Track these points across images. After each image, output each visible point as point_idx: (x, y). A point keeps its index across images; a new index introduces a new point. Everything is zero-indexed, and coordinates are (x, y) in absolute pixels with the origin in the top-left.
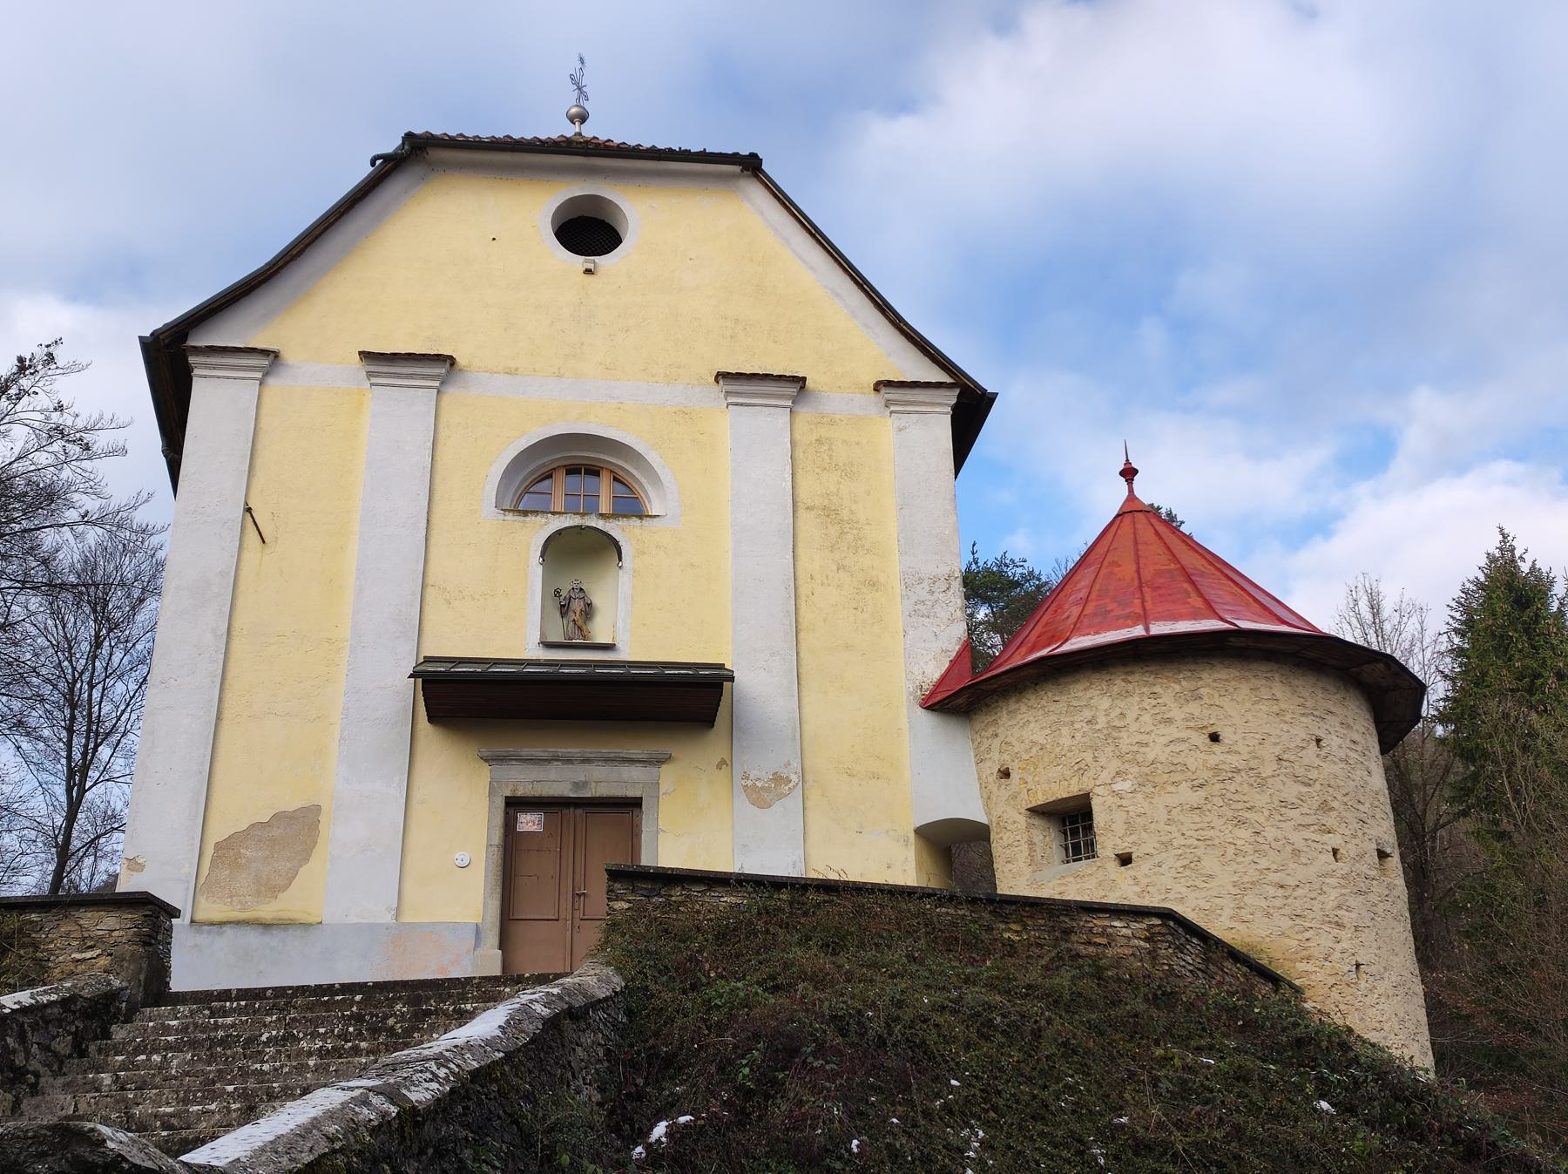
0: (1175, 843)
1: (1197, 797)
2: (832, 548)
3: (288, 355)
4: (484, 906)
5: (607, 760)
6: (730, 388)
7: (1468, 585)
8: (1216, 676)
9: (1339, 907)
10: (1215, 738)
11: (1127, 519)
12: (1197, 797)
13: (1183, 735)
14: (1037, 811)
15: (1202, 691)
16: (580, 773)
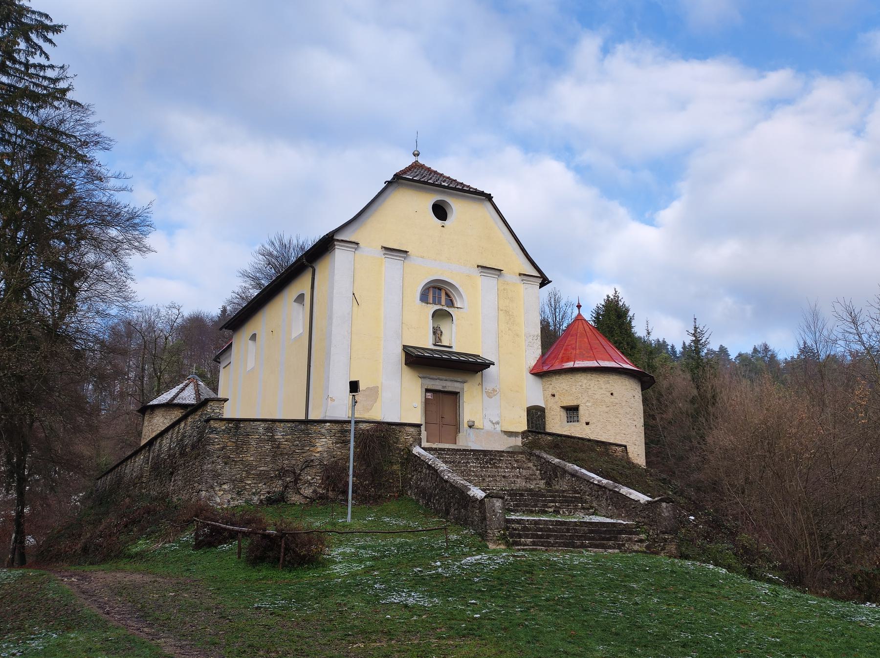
0: (601, 421)
1: (607, 410)
2: (507, 323)
3: (361, 245)
4: (421, 418)
5: (452, 381)
6: (482, 270)
7: (599, 305)
8: (613, 377)
9: (635, 440)
10: (612, 394)
11: (577, 321)
12: (607, 410)
13: (605, 392)
14: (562, 407)
15: (610, 381)
16: (444, 383)
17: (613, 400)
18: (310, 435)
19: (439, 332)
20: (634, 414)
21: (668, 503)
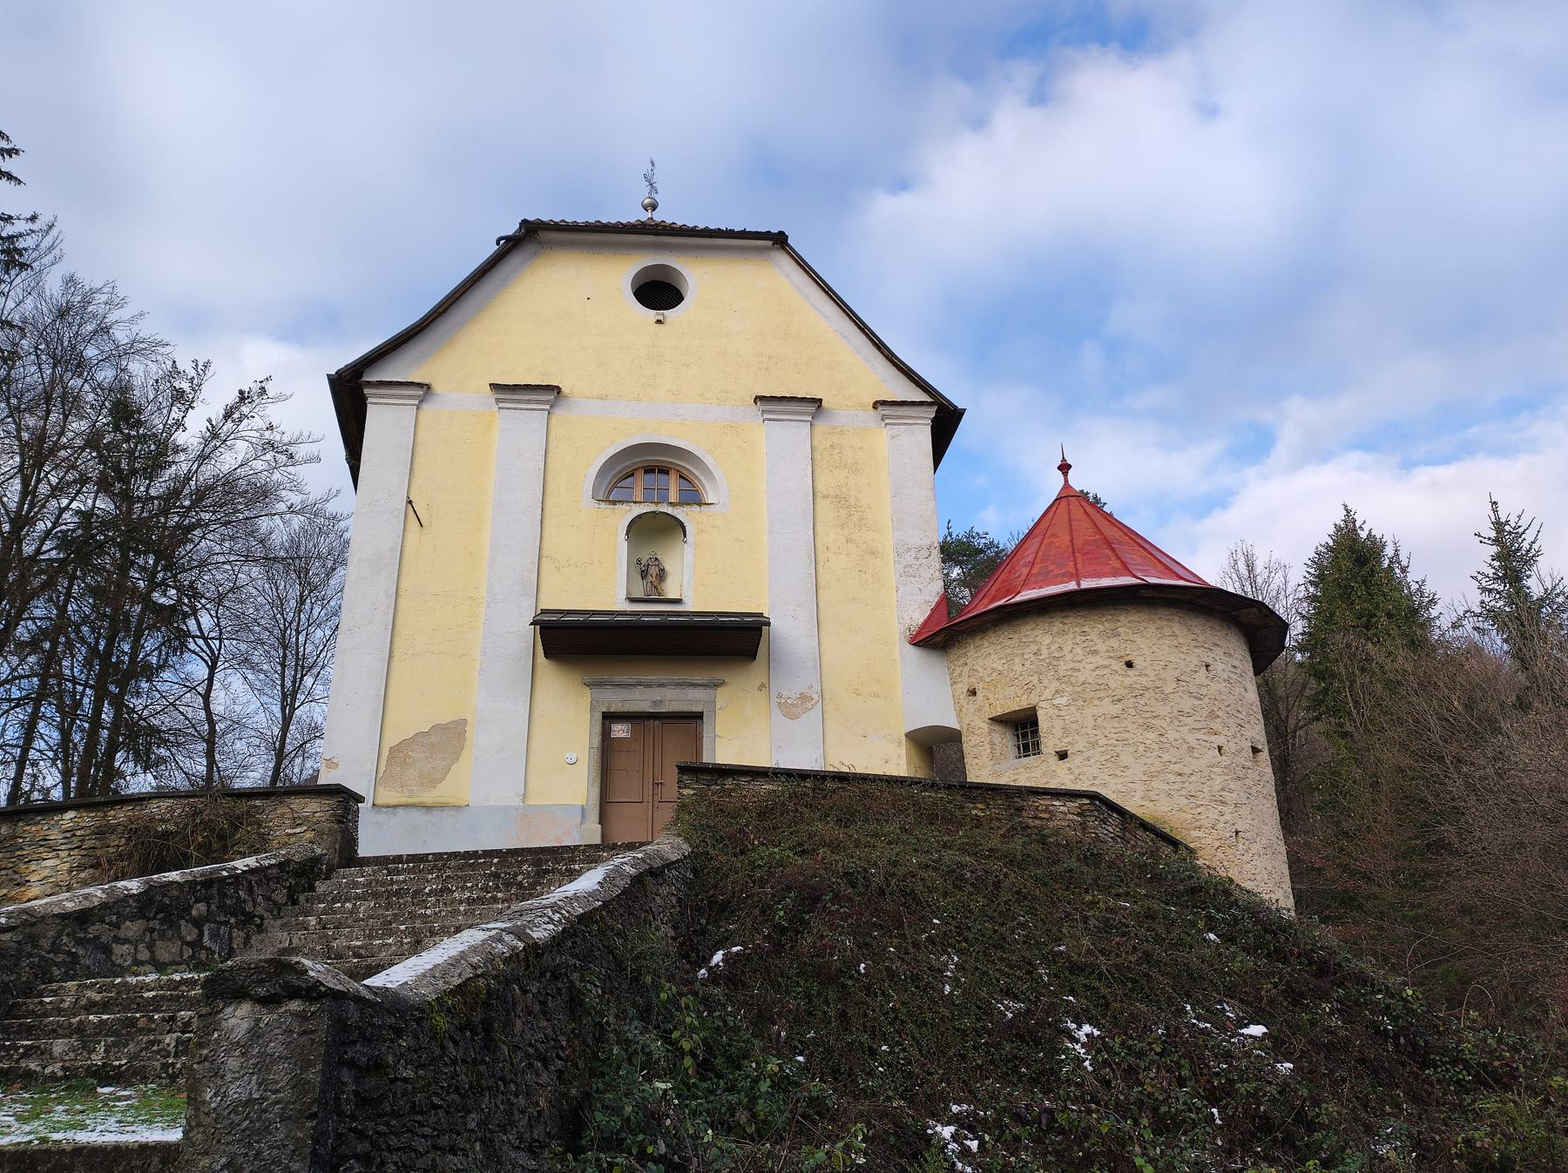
1: (1115, 709)
2: (842, 527)
3: (437, 387)
5: (678, 685)
6: (765, 408)
7: (1320, 548)
8: (1130, 618)
9: (1223, 789)
10: (1129, 665)
11: (1064, 503)
12: (1115, 709)
13: (1106, 663)
14: (996, 720)
16: (657, 694)
17: (1135, 679)
18: (18, 853)
19: (653, 571)
20: (1212, 715)
21: (270, 1001)
